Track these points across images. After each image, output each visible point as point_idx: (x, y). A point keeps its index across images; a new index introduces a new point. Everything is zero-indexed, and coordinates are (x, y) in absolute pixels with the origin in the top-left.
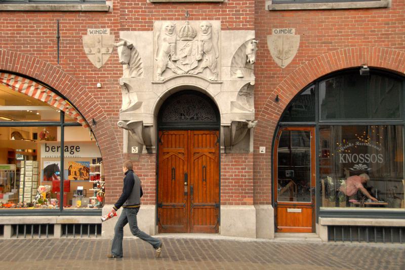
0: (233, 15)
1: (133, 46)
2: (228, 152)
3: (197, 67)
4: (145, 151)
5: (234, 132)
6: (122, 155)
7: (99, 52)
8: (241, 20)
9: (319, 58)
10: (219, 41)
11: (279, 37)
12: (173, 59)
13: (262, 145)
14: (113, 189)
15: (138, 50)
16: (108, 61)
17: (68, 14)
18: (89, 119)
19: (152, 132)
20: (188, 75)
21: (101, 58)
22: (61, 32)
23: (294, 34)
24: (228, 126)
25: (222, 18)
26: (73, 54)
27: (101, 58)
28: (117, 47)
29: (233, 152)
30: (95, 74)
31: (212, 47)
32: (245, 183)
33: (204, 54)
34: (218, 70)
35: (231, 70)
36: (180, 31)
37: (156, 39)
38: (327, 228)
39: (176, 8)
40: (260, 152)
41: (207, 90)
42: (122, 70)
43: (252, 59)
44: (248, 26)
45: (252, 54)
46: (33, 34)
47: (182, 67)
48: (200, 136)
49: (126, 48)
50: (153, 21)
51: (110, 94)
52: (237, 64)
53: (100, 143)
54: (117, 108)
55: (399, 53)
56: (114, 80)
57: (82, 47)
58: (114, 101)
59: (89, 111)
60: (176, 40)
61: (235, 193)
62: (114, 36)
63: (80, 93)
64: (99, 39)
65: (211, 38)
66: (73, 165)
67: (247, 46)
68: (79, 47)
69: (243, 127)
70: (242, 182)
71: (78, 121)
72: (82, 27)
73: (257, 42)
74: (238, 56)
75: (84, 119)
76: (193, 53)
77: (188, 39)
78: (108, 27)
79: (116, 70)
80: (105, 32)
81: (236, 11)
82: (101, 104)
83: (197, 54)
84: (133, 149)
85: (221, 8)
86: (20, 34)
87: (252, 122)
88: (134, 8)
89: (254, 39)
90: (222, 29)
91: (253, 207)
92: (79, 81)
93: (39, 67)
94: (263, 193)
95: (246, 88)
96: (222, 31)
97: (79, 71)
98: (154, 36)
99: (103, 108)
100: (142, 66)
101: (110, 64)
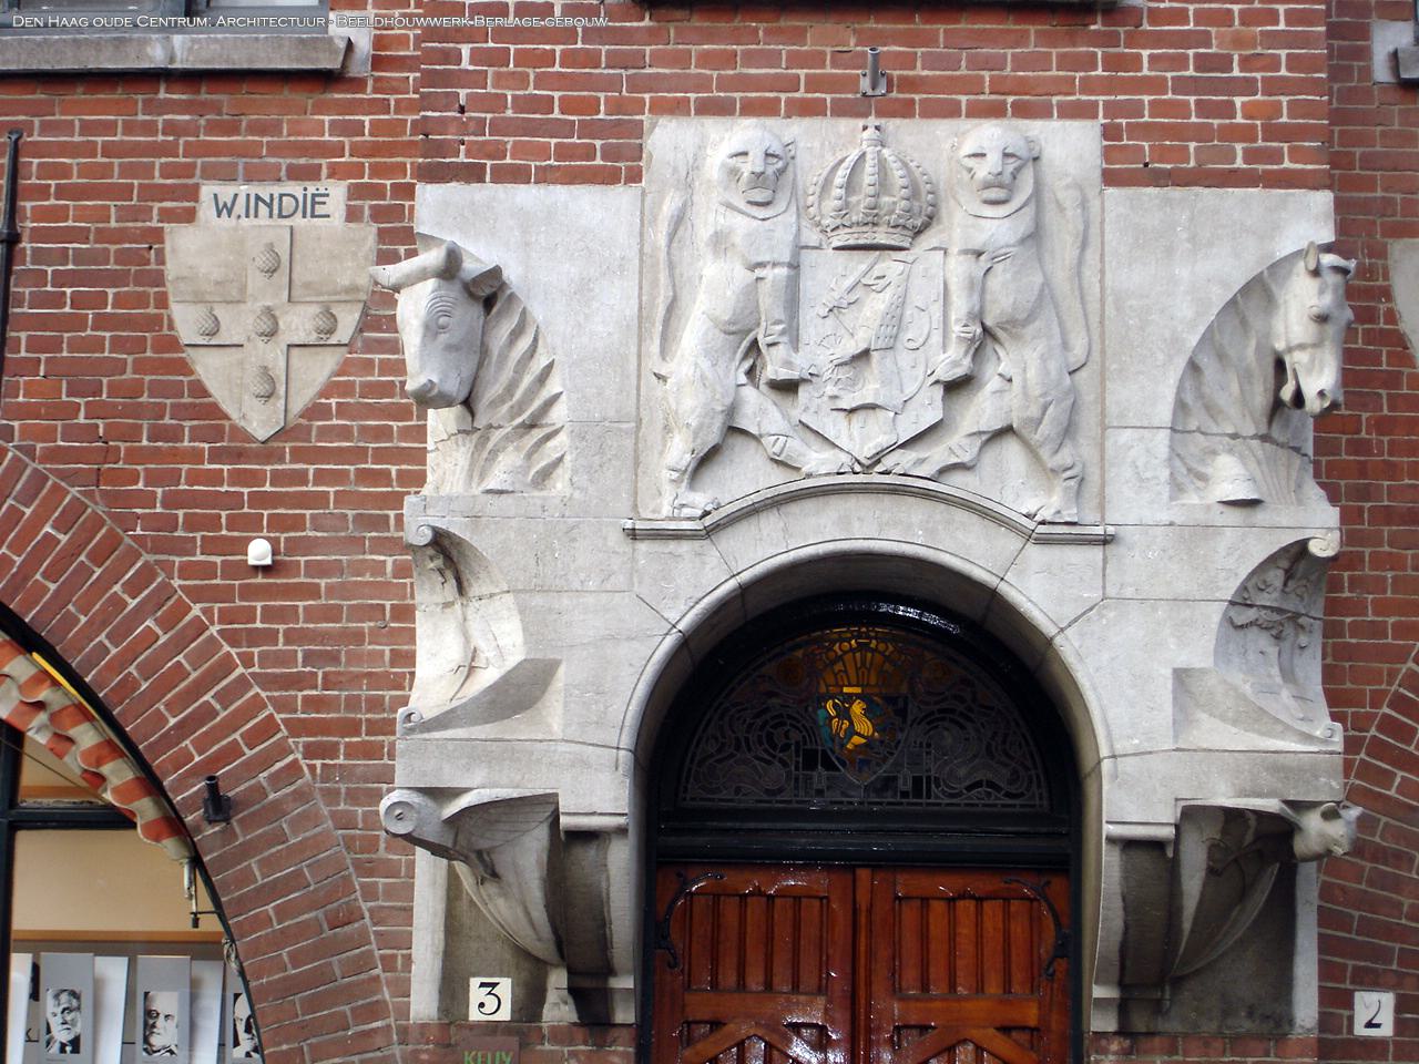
0: (1182, 85)
1: (503, 285)
2: (1140, 1023)
3: (933, 429)
4: (558, 1010)
5: (1193, 883)
6: (404, 1032)
7: (271, 334)
8: (1239, 119)
10: (1092, 256)
12: (774, 369)
13: (1373, 982)
15: (538, 312)
17: (79, 94)
18: (182, 784)
19: (619, 867)
21: (280, 374)
22: (28, 205)
24: (1156, 845)
25: (1112, 110)
26: (98, 345)
27: (280, 374)
28: (397, 289)
29: (1173, 1025)
30: (239, 478)
31: (1046, 294)
33: (985, 338)
34: (1082, 451)
36: (827, 185)
37: (662, 241)
38: (194, 962)
39: (798, 36)
40: (1360, 1030)
41: (1003, 588)
42: (420, 456)
43: (1319, 378)
44: (1287, 164)
45: (1317, 345)
47: (833, 426)
48: (938, 907)
49: (453, 292)
50: (646, 118)
51: (332, 614)
52: (1211, 410)
53: (255, 949)
54: (375, 704)
56: (365, 522)
57: (162, 301)
58: (354, 658)
59: (184, 729)
60: (799, 247)
62: (374, 227)
63: (132, 603)
64: (271, 248)
65: (1035, 237)
66: (909, 368)
68: (141, 301)
71: (108, 796)
72: (167, 171)
73: (1352, 264)
74: (1221, 357)
75: (151, 783)
76: (914, 332)
77: (882, 239)
78: (334, 173)
79: (380, 456)
80: (311, 207)
81: (1203, 63)
82: (267, 682)
83: (936, 338)
84: (476, 993)
87: (1331, 815)
88: (516, 34)
89: (1328, 248)
90: (1110, 178)
92: (127, 523)
95: (1276, 577)
96: (1111, 191)
97: (135, 456)
98: (645, 220)
99: (281, 705)
100: (558, 414)
101: (343, 410)
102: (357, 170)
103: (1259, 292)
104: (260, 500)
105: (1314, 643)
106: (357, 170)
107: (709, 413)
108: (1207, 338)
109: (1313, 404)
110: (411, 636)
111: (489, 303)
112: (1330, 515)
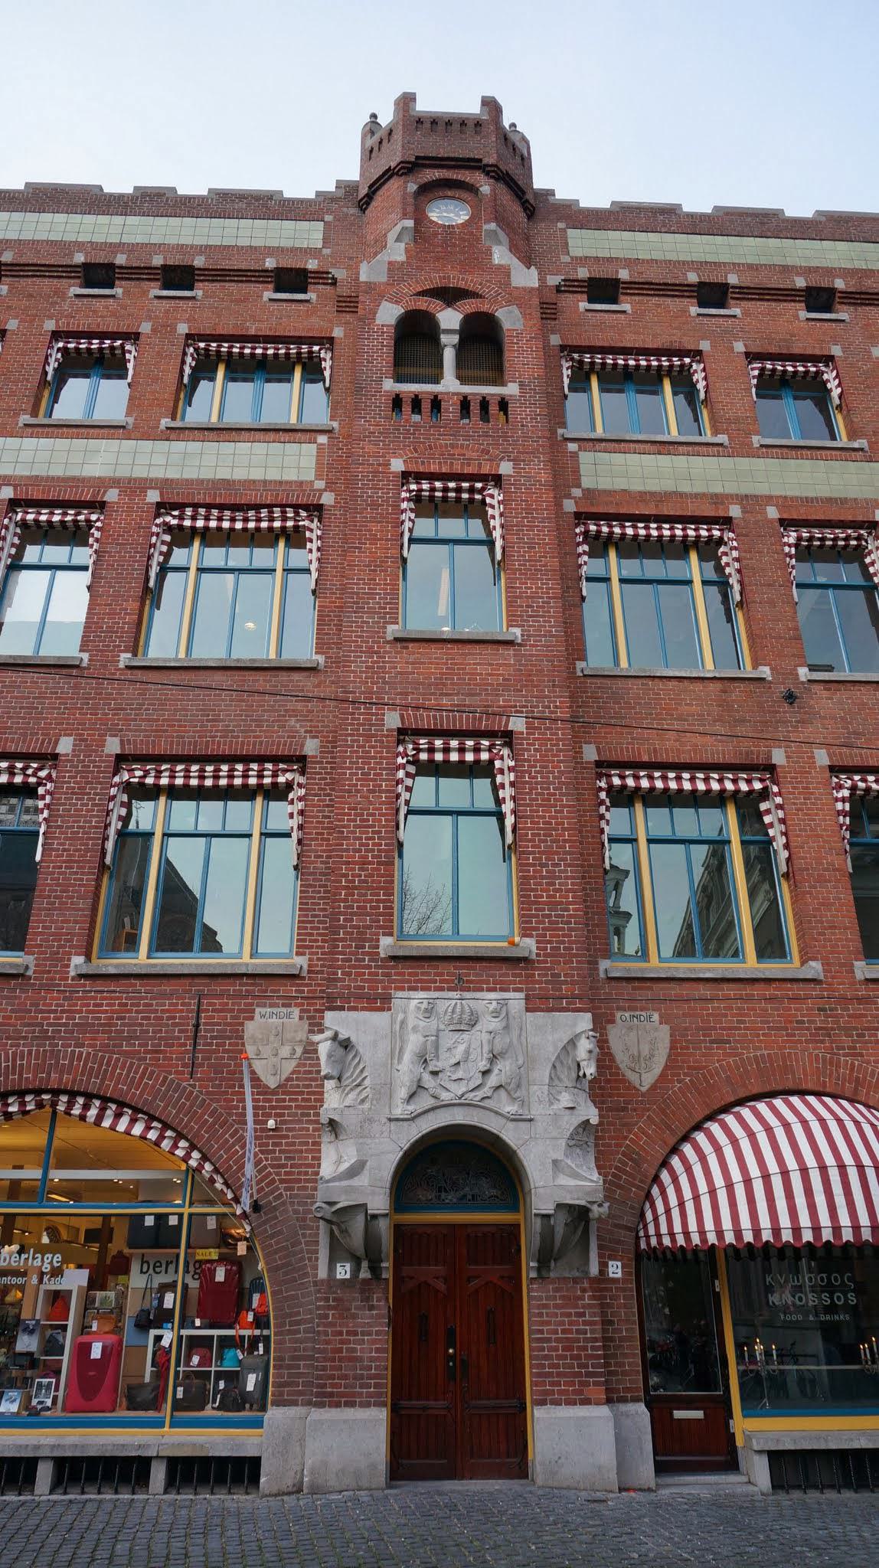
0: (546, 982)
2: (545, 1274)
4: (364, 1274)
5: (560, 1231)
6: (315, 1283)
9: (709, 1071)
10: (524, 1034)
11: (630, 1028)
12: (431, 1068)
14: (289, 1367)
15: (361, 1050)
16: (292, 1073)
19: (384, 1227)
20: (462, 1101)
23: (658, 1022)
25: (527, 990)
32: (585, 1348)
33: (494, 1058)
35: (550, 1093)
40: (611, 1275)
41: (501, 1135)
43: (590, 1070)
46: (149, 1018)
51: (293, 1144)
52: (559, 1079)
55: (853, 1064)
57: (243, 1045)
60: (438, 1030)
61: (564, 1375)
67: (578, 1044)
68: (237, 1044)
69: (579, 1215)
70: (579, 1348)
74: (562, 1063)
78: (296, 1005)
79: (309, 1093)
80: (289, 1016)
81: (553, 975)
82: (273, 1166)
84: (339, 1269)
85: (523, 969)
86: (123, 1018)
87: (600, 1205)
90: (528, 1010)
91: (604, 1411)
92: (230, 1115)
93: (153, 1086)
94: (624, 1373)
98: (393, 1021)
99: (278, 1174)
100: (367, 1082)
101: (298, 1079)
102: (303, 1004)
103: (572, 1042)
104: (272, 1108)
105: (592, 1150)
106: (303, 1004)
107: (412, 1082)
108: (558, 1057)
109: (589, 1077)
110: (319, 1151)
111: (346, 1047)
112: (596, 1111)
